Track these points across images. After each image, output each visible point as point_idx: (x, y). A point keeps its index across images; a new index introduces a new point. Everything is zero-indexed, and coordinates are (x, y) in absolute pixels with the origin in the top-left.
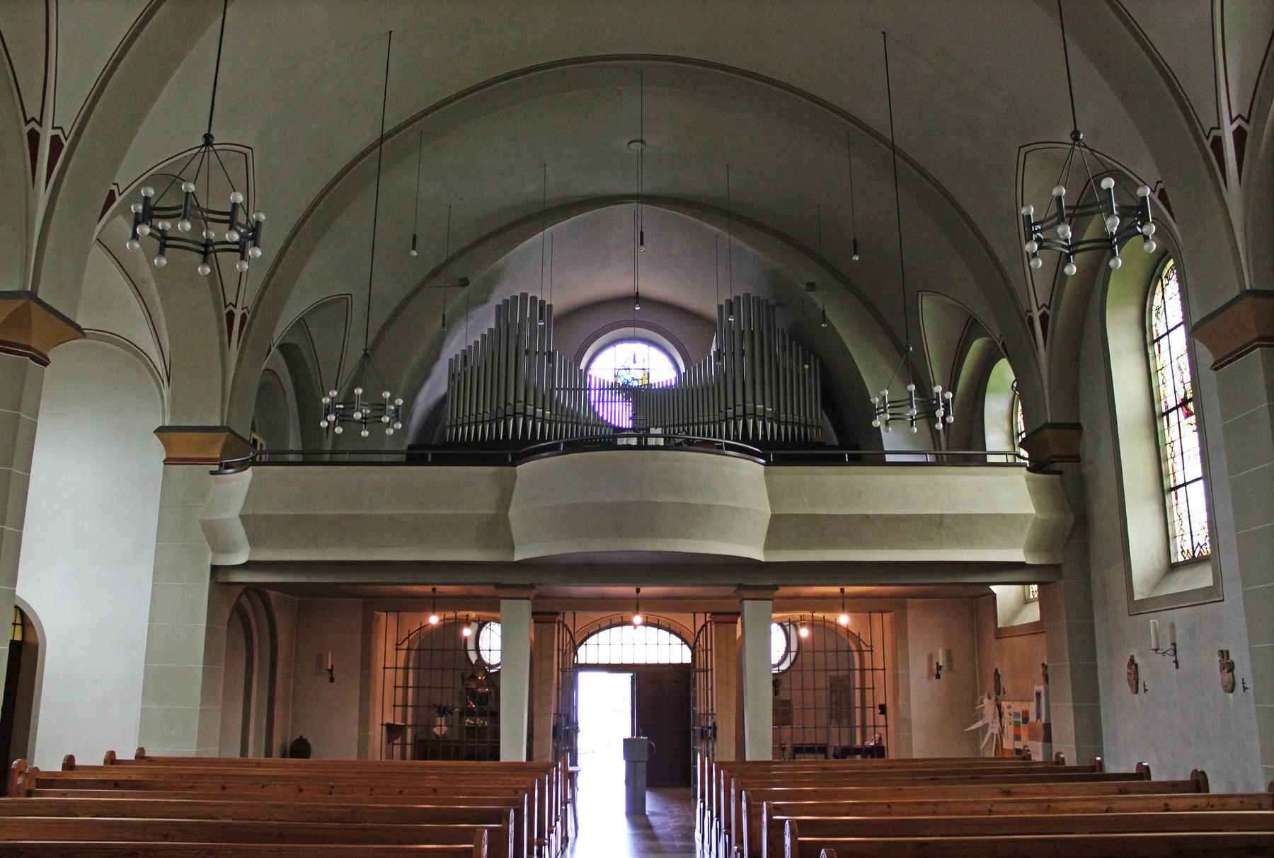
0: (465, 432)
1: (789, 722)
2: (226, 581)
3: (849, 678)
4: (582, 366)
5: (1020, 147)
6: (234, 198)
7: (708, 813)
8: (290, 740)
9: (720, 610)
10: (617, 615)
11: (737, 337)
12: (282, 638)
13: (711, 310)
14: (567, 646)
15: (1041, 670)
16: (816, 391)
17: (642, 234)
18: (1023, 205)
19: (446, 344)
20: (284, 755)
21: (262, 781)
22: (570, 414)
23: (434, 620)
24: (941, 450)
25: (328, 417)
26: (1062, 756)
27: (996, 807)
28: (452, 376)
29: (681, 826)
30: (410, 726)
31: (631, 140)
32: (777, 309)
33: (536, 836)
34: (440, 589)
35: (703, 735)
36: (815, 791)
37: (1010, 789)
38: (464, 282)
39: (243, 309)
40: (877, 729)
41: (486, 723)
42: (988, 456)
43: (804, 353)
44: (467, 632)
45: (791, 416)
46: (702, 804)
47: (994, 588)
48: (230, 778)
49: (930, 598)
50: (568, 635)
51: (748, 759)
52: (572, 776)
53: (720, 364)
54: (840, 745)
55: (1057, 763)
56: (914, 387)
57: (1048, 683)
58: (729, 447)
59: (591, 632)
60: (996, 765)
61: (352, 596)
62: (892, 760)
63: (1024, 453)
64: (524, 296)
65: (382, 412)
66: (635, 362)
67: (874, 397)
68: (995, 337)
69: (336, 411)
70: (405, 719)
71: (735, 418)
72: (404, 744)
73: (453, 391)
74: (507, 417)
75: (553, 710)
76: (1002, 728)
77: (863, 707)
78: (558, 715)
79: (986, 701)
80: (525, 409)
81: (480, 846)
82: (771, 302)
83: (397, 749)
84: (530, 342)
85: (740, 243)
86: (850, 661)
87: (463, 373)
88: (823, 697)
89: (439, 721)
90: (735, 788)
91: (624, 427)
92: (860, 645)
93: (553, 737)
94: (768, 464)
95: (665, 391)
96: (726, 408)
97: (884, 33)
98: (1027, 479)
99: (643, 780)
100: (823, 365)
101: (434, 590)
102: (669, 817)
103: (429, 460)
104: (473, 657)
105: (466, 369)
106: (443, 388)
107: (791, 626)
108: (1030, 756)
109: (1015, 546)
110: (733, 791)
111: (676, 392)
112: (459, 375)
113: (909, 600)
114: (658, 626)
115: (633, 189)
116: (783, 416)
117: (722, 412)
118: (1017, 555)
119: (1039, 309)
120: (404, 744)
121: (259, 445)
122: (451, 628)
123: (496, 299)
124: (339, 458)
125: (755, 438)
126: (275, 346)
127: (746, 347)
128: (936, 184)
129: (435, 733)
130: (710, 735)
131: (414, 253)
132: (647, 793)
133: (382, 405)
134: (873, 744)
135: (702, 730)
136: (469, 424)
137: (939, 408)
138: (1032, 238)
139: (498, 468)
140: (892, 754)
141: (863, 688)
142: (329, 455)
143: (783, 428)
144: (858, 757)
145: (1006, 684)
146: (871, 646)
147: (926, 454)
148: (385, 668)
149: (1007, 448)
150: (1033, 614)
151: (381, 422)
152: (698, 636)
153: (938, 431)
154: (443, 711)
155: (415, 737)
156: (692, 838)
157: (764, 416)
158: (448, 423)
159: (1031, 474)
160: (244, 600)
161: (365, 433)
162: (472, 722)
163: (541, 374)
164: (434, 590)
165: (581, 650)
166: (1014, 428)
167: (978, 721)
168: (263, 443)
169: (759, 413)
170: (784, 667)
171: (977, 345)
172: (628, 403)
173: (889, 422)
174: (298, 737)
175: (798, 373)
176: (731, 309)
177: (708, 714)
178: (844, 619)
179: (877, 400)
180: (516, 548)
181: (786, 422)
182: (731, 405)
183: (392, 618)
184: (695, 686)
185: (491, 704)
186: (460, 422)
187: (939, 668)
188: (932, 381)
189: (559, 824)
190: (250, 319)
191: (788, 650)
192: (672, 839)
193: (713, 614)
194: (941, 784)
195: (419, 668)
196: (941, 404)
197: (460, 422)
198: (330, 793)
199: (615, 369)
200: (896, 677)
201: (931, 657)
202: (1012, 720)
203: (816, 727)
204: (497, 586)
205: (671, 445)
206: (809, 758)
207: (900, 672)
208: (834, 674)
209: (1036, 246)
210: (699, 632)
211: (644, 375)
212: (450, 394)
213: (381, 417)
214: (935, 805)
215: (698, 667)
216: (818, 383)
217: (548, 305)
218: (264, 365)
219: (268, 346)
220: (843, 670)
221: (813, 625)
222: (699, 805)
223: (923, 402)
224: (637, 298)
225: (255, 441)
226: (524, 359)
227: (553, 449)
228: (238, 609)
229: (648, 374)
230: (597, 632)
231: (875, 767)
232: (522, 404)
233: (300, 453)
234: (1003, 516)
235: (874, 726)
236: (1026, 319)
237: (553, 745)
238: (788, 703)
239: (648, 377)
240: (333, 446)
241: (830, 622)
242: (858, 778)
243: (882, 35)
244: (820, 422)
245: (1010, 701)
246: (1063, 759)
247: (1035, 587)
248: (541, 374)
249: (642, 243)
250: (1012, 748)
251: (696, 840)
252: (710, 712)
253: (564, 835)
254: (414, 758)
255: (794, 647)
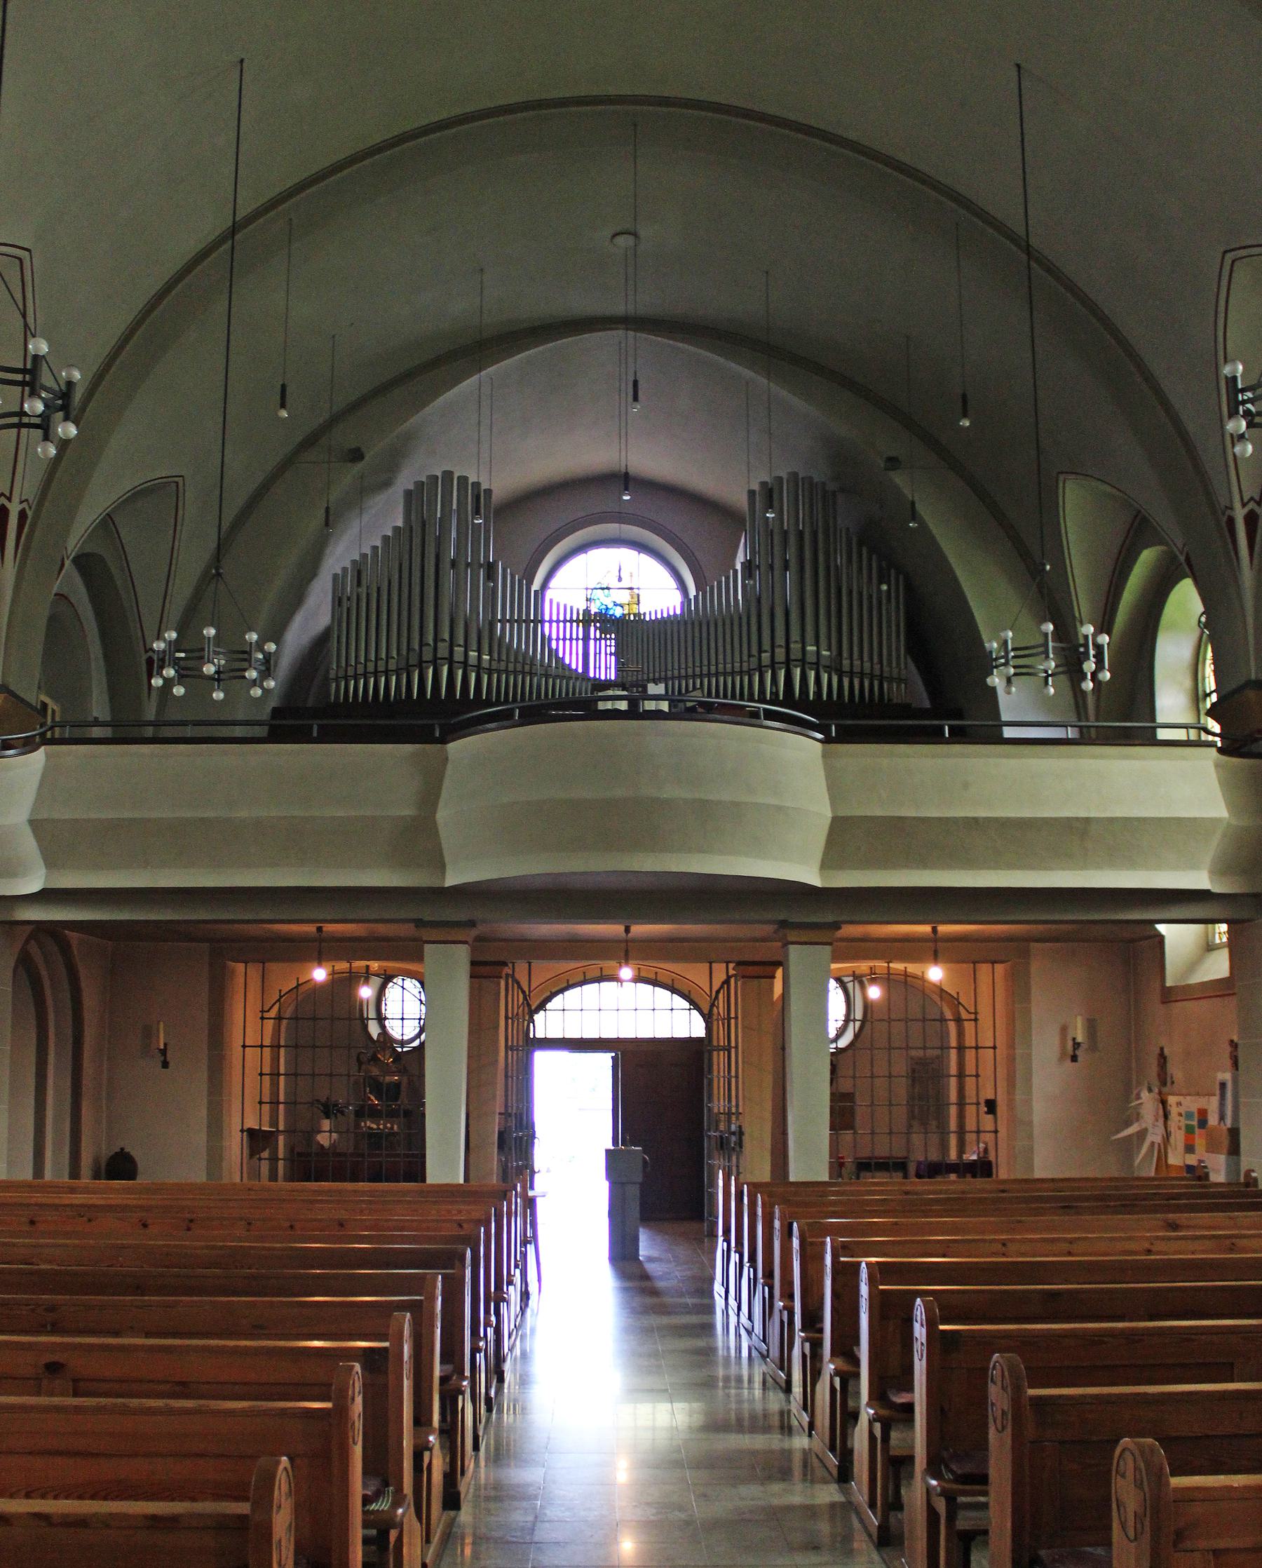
0: (358, 688)
1: (850, 1126)
2: (9, 918)
3: (941, 1060)
4: (536, 586)
5: (1225, 252)
6: (35, 348)
7: (734, 1257)
8: (106, 1152)
9: (747, 958)
10: (594, 966)
11: (777, 539)
12: (90, 1001)
13: (737, 496)
14: (518, 1008)
15: (1228, 1049)
16: (898, 626)
17: (635, 383)
18: (1226, 361)
19: (328, 551)
20: (96, 1176)
21: (88, 1213)
22: (520, 659)
23: (320, 974)
24: (1088, 720)
25: (164, 672)
26: (1254, 1175)
27: (1158, 1246)
28: (338, 601)
29: (693, 1277)
30: (282, 1131)
31: (619, 229)
32: (840, 499)
33: (493, 1289)
34: (328, 928)
35: (722, 1144)
36: (896, 1223)
37: (1178, 1222)
38: (356, 455)
39: (21, 502)
40: (982, 1135)
41: (395, 1127)
42: (1004, 728)
43: (880, 569)
44: (366, 992)
45: (859, 662)
46: (725, 1244)
47: (1161, 928)
48: (37, 1208)
49: (1066, 941)
50: (521, 996)
51: (792, 1179)
52: (530, 1203)
53: (752, 582)
54: (926, 1158)
55: (1247, 1185)
56: (1051, 627)
57: (1237, 1069)
58: (770, 715)
59: (553, 990)
60: (1157, 1187)
61: (192, 940)
62: (1005, 1181)
63: (1215, 727)
64: (448, 475)
65: (245, 664)
66: (620, 579)
67: (990, 641)
68: (1175, 545)
69: (176, 663)
70: (274, 1121)
71: (773, 665)
72: (274, 1159)
73: (340, 626)
74: (424, 665)
75: (499, 1108)
76: (1167, 1136)
77: (961, 1104)
78: (506, 1115)
79: (1145, 1095)
80: (451, 652)
81: (432, 1299)
82: (831, 486)
83: (265, 1167)
84: (458, 547)
85: (784, 393)
86: (944, 1035)
87: (355, 597)
88: (901, 1089)
89: (326, 1124)
90: (781, 1219)
91: (603, 678)
92: (959, 1013)
93: (499, 1148)
94: (827, 740)
95: (663, 626)
96: (760, 651)
97: (1018, 66)
98: (1217, 766)
99: (634, 1210)
100: (909, 588)
101: (320, 929)
102: (674, 1264)
103: (315, 734)
104: (374, 1030)
105: (360, 590)
106: (324, 619)
107: (856, 982)
108: (1207, 1175)
109: (1193, 866)
110: (777, 1224)
111: (689, 627)
112: (349, 599)
113: (1032, 944)
114: (655, 983)
115: (619, 309)
116: (846, 663)
117: (754, 656)
118: (1199, 880)
119: (1244, 505)
120: (274, 1159)
121: (50, 712)
122: (344, 984)
123: (405, 480)
124: (168, 732)
125: (804, 697)
126: (71, 558)
127: (791, 555)
128: (1094, 309)
129: (319, 1142)
130: (731, 1145)
131: (284, 414)
132: (641, 1230)
133: (245, 652)
134: (974, 1157)
135: (721, 1137)
136: (376, 674)
137: (1089, 659)
138: (1237, 412)
139: (418, 746)
140: (1003, 1173)
141: (961, 1075)
142: (151, 728)
143: (846, 681)
144: (953, 1177)
145: (1176, 1071)
146: (976, 1013)
147: (1066, 726)
148: (244, 1046)
149: (1188, 718)
150: (1218, 967)
151: (244, 677)
152: (717, 998)
153: (1084, 693)
154: (329, 1110)
155: (291, 1149)
156: (710, 1294)
157: (817, 664)
158: (332, 674)
159: (1225, 759)
160: (34, 949)
161: (218, 695)
162: (375, 1126)
163: (475, 599)
164: (320, 929)
165: (539, 1018)
166: (1200, 685)
167: (1131, 1125)
168: (55, 708)
169: (811, 658)
170: (842, 1043)
171: (1147, 558)
172: (608, 642)
173: (1014, 679)
174: (118, 1150)
175: (870, 597)
176: (771, 497)
177: (729, 1114)
178: (935, 974)
179: (995, 645)
180: (448, 867)
181: (851, 674)
182: (766, 645)
183: (254, 971)
184: (710, 1071)
185: (404, 1101)
186: (351, 672)
187: (1076, 1045)
188: (1077, 615)
189: (518, 1271)
190: (33, 517)
191: (847, 1020)
192: (682, 1295)
193: (739, 964)
194: (1078, 1213)
195: (296, 1046)
196: (1092, 652)
197: (351, 672)
198: (189, 1229)
199: (587, 589)
200: (1011, 1060)
201: (1064, 1030)
202: (1183, 1122)
203: (890, 1133)
204: (419, 923)
205: (683, 711)
206: (880, 1178)
207: (1019, 1052)
208: (920, 1053)
209: (1244, 423)
210: (718, 992)
211: (632, 598)
212: (336, 628)
213: (245, 670)
214: (1071, 1243)
215: (715, 1043)
216: (902, 614)
217: (473, 483)
218: (55, 590)
219: (59, 559)
220: (933, 1048)
221: (887, 980)
222: (721, 1245)
223: (1063, 649)
224: (625, 480)
225: (45, 705)
226: (449, 576)
227: (503, 719)
228: (24, 962)
229: (638, 595)
230: (562, 991)
231: (983, 1191)
232: (447, 644)
233: (107, 726)
234: (1179, 821)
235: (978, 1132)
236: (1225, 519)
237: (500, 1161)
238: (849, 1097)
239: (638, 600)
240: (158, 713)
241: (915, 977)
242: (957, 1205)
243: (1015, 69)
244: (904, 672)
245: (1181, 1095)
246: (1256, 1180)
247: (1224, 927)
248: (475, 599)
249: (636, 398)
250: (1182, 1164)
251: (716, 1296)
252: (734, 1110)
253: (523, 1290)
254: (290, 1178)
255: (859, 1014)
